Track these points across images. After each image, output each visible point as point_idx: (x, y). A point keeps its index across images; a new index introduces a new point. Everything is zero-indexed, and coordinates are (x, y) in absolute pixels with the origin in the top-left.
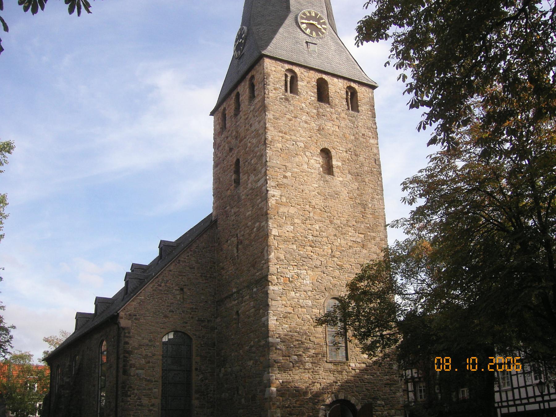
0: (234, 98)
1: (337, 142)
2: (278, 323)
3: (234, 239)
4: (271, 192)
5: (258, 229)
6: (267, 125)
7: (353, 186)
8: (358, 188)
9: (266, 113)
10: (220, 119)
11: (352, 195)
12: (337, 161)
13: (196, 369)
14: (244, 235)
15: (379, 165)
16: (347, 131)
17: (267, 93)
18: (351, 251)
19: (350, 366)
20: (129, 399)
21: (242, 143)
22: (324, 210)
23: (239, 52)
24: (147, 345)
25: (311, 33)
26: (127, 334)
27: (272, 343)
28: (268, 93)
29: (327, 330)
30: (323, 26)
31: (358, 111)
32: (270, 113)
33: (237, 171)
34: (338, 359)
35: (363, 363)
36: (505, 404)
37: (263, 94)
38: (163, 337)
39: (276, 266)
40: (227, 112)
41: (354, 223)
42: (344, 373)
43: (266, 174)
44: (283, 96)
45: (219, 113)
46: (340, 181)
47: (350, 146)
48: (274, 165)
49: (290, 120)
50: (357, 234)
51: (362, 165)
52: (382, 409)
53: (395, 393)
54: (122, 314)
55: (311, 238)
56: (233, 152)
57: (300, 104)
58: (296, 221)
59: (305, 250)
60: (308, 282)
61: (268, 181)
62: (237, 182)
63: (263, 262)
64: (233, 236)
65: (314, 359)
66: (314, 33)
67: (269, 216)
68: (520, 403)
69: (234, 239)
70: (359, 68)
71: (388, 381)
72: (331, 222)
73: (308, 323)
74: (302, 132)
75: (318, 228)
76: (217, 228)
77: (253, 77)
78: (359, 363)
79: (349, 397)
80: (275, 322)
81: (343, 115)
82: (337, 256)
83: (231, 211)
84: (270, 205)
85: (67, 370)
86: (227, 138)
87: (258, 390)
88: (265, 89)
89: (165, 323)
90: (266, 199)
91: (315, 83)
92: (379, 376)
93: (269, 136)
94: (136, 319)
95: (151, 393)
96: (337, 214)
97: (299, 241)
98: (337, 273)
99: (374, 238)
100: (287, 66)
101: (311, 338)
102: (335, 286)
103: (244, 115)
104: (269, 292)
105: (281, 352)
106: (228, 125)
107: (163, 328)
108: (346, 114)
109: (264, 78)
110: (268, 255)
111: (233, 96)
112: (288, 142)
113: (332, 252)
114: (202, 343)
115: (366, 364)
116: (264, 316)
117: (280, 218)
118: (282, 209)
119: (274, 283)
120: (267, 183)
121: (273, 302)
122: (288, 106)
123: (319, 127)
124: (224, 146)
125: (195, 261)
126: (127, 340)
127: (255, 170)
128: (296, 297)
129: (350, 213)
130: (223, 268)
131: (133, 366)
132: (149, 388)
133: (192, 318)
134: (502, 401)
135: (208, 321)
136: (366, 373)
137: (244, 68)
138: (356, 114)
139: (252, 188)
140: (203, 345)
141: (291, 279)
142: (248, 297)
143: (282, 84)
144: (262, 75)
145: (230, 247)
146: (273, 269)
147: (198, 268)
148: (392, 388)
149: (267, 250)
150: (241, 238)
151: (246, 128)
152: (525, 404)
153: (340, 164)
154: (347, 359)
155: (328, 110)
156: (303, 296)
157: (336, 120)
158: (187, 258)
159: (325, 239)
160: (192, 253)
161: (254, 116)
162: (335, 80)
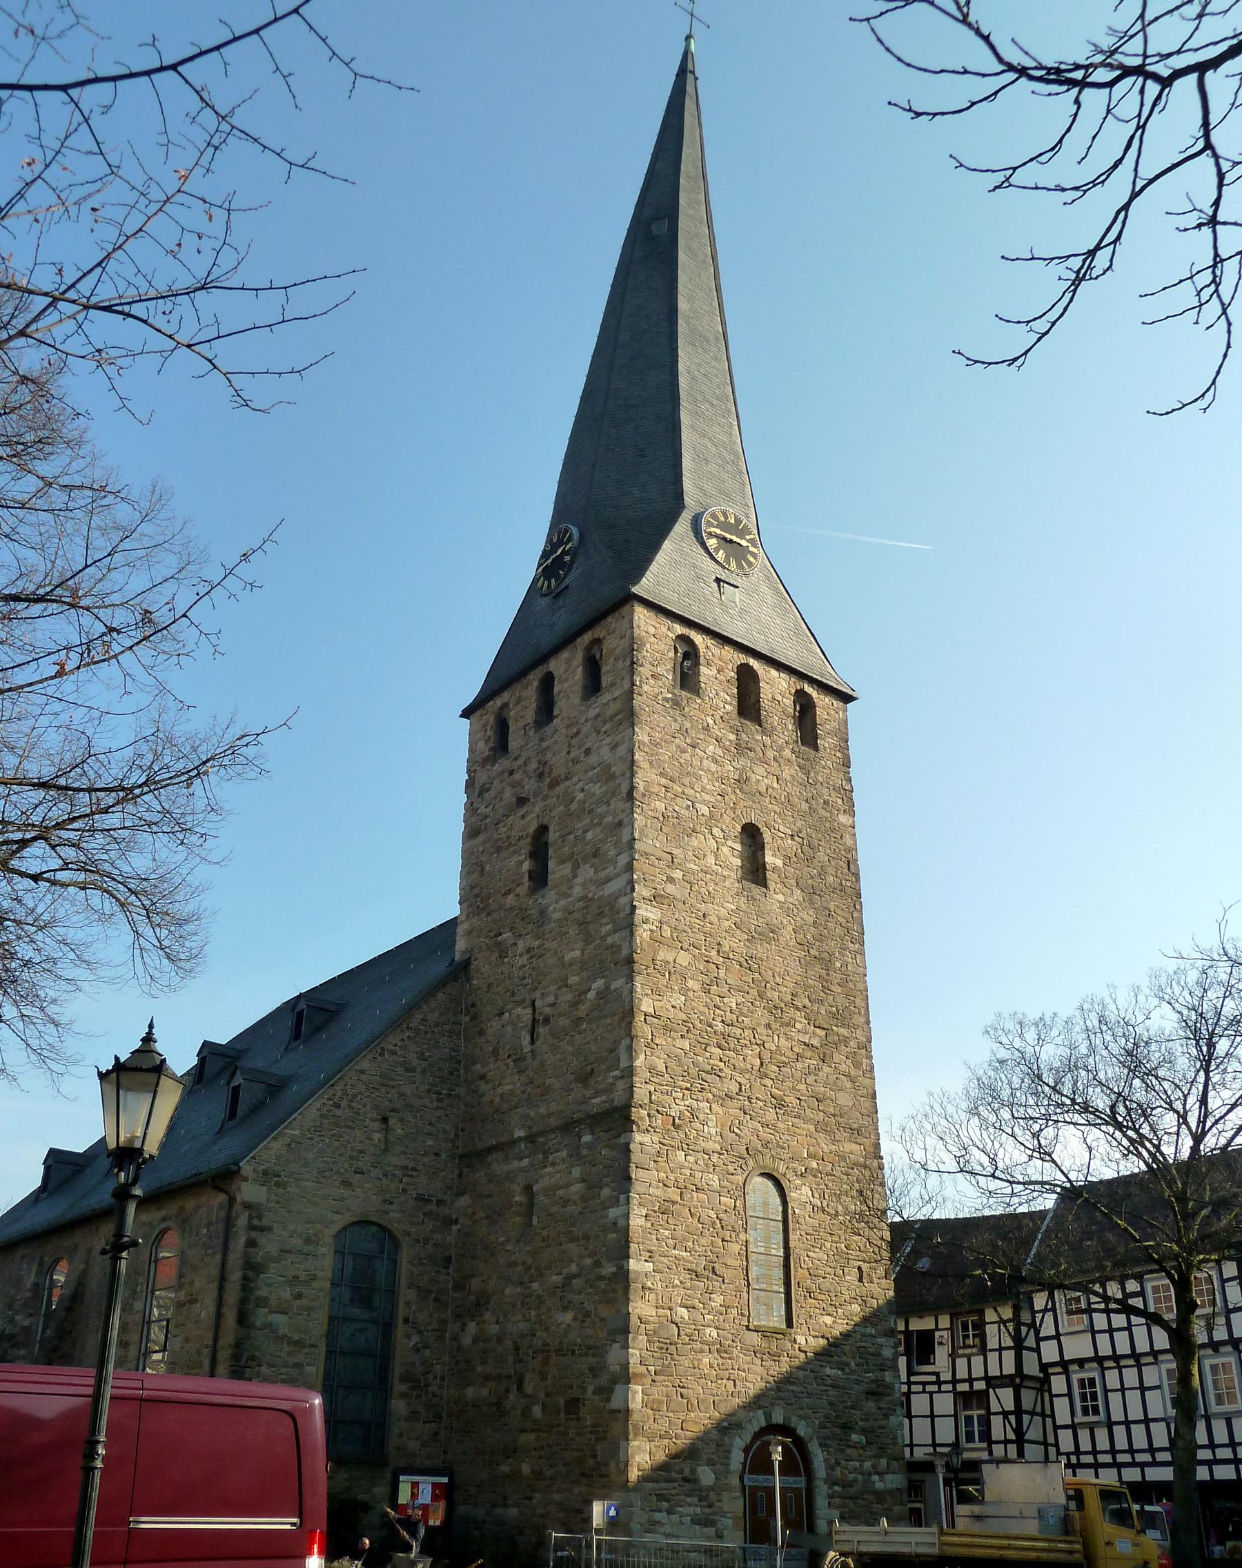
0: (535, 684)
4: (644, 911)
7: (805, 917)
9: (636, 729)
10: (489, 728)
13: (406, 1321)
14: (555, 1004)
15: (857, 875)
17: (638, 683)
18: (800, 1065)
19: (795, 1341)
21: (557, 789)
22: (749, 963)
23: (553, 581)
24: (300, 1252)
25: (727, 560)
26: (255, 1222)
27: (635, 1272)
31: (816, 748)
34: (771, 1324)
35: (823, 1337)
36: (1088, 1459)
39: (648, 1086)
41: (806, 1002)
43: (630, 868)
44: (670, 696)
45: (487, 713)
46: (779, 902)
51: (822, 872)
52: (860, 1456)
53: (886, 1416)
54: (246, 1168)
55: (719, 1027)
60: (713, 1131)
62: (539, 878)
63: (617, 1073)
64: (520, 1003)
65: (721, 1318)
66: (733, 563)
67: (636, 967)
68: (1150, 1460)
69: (525, 1013)
70: (819, 651)
71: (874, 1386)
72: (761, 996)
73: (711, 1229)
74: (705, 781)
75: (734, 1006)
76: (468, 980)
79: (794, 1419)
80: (641, 1221)
81: (787, 753)
82: (772, 1075)
83: (515, 944)
85: (29, 1294)
86: (511, 773)
87: (590, 1389)
88: (633, 674)
89: (342, 1199)
90: (629, 925)
92: (855, 1371)
93: (640, 782)
94: (278, 1184)
95: (298, 1375)
98: (771, 1115)
99: (846, 1041)
100: (679, 629)
102: (766, 1145)
103: (568, 727)
104: (632, 1146)
105: (653, 1296)
106: (514, 743)
107: (337, 1213)
110: (631, 1058)
111: (534, 679)
113: (762, 1064)
114: (423, 1255)
115: (828, 1339)
116: (615, 1202)
117: (658, 975)
118: (664, 955)
120: (633, 890)
122: (679, 719)
124: (502, 792)
125: (416, 1052)
127: (595, 855)
128: (686, 1164)
129: (799, 978)
130: (483, 1077)
131: (262, 1302)
132: (296, 1364)
133: (404, 1191)
135: (440, 1202)
136: (829, 1362)
137: (564, 619)
139: (587, 897)
140: (424, 1261)
141: (677, 1121)
142: (564, 1153)
143: (669, 667)
144: (625, 643)
147: (424, 1072)
148: (883, 1405)
150: (547, 1010)
151: (572, 755)
152: (1142, 1465)
153: (779, 863)
154: (790, 1323)
156: (701, 1162)
158: (399, 1044)
159: (747, 1032)
160: (412, 1035)
162: (774, 673)
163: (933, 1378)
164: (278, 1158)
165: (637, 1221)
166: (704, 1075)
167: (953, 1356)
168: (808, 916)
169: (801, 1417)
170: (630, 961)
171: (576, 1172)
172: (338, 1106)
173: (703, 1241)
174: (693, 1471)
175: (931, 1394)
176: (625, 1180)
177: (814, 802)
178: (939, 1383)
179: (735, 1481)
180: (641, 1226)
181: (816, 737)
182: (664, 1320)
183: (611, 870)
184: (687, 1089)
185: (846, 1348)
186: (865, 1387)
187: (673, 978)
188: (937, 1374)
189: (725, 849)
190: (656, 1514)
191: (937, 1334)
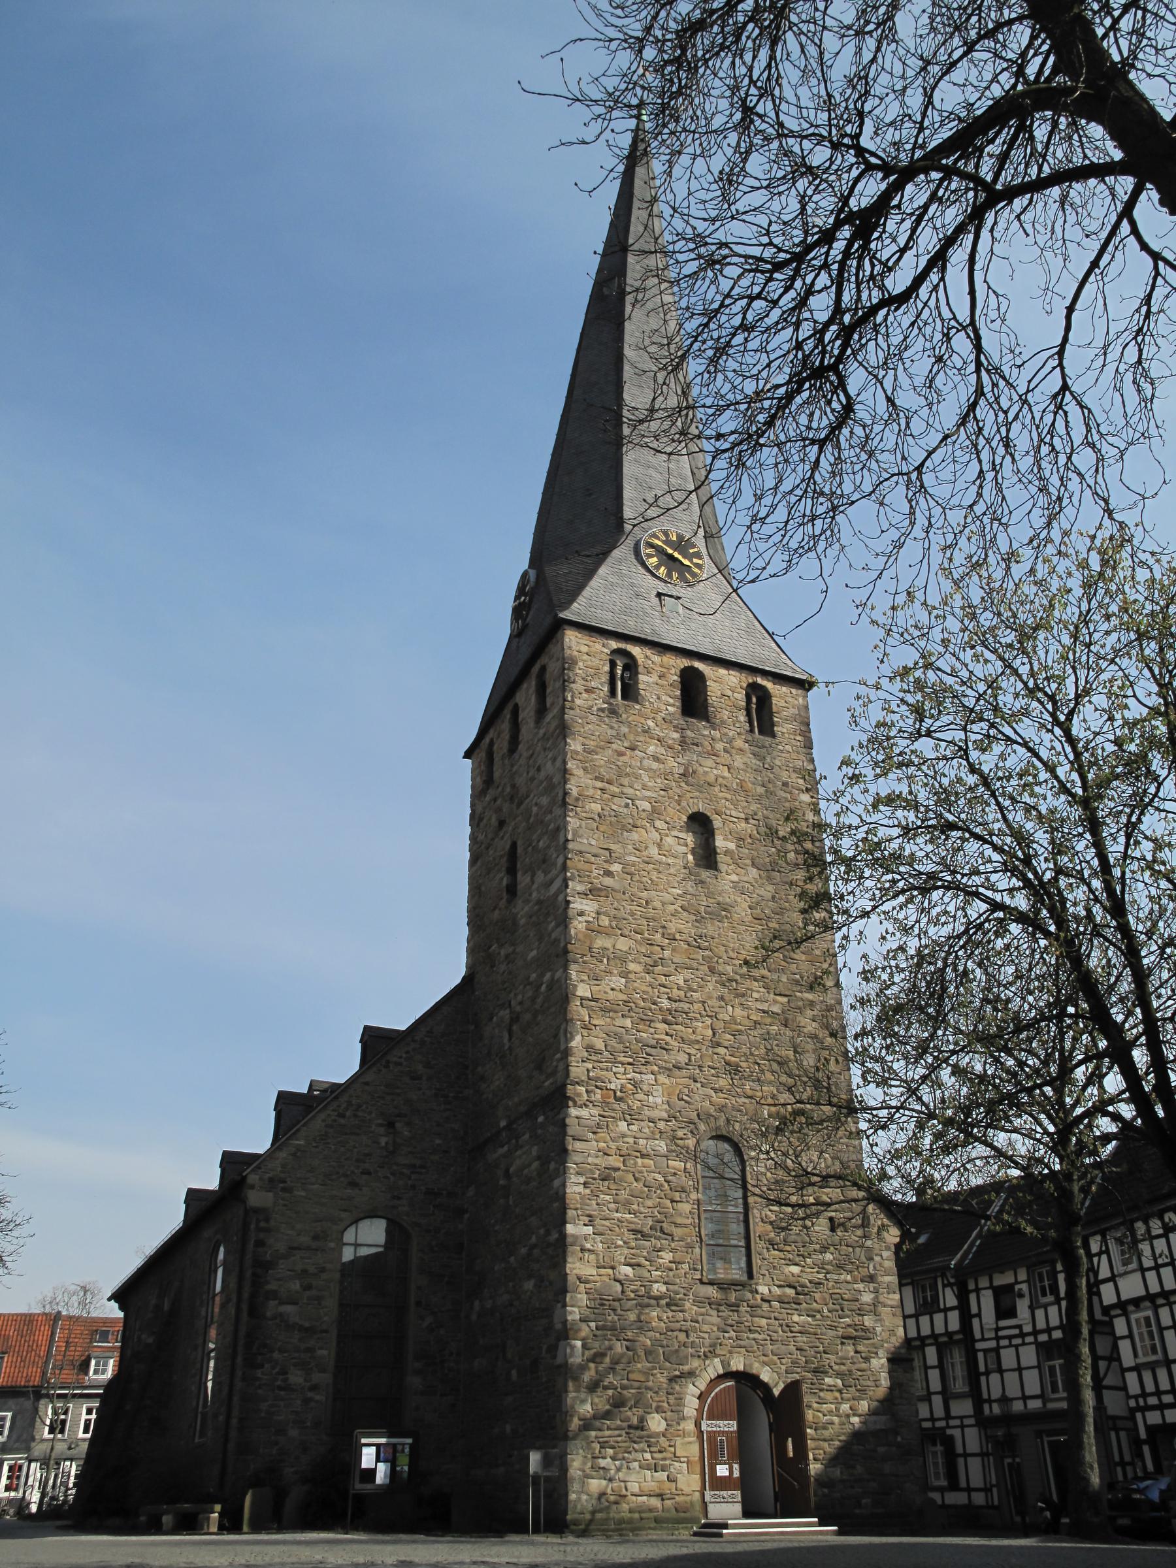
0: (508, 716)
1: (726, 799)
2: (588, 1191)
3: (505, 1014)
4: (577, 904)
5: (550, 987)
6: (569, 765)
7: (762, 892)
8: (773, 897)
11: (759, 911)
12: (726, 839)
13: (418, 1304)
16: (748, 777)
20: (259, 1373)
21: (522, 807)
24: (308, 1248)
25: (669, 575)
26: (262, 1224)
27: (573, 1235)
28: (573, 701)
29: (702, 1208)
30: (695, 561)
31: (773, 735)
32: (574, 739)
33: (512, 870)
34: (730, 1277)
35: (790, 1286)
36: (1153, 1401)
37: (561, 702)
38: (345, 1230)
40: (495, 748)
42: (744, 1308)
43: (565, 868)
47: (754, 807)
48: (583, 848)
49: (621, 754)
50: (772, 996)
53: (867, 1359)
55: (665, 1003)
56: (504, 829)
57: (643, 721)
58: (632, 966)
59: (652, 1030)
60: (659, 1100)
61: (570, 883)
62: (512, 890)
63: (558, 1056)
64: (502, 1006)
65: (671, 1274)
66: (675, 575)
67: (570, 956)
69: (505, 1014)
71: (851, 1330)
72: (712, 970)
74: (646, 778)
75: (681, 982)
77: (543, 669)
78: (779, 1286)
80: (580, 1189)
81: (739, 743)
82: (726, 1043)
84: (573, 932)
88: (564, 690)
90: (564, 921)
91: (676, 678)
93: (573, 788)
94: (284, 1190)
96: (727, 952)
97: (637, 1010)
98: (723, 1082)
99: (812, 1004)
100: (614, 644)
101: (665, 1225)
104: (568, 1121)
105: (592, 1257)
107: (345, 1210)
108: (746, 741)
109: (564, 669)
110: (568, 1041)
111: (507, 714)
112: (616, 800)
113: (714, 1034)
116: (557, 1176)
118: (600, 942)
119: (579, 1103)
120: (567, 886)
121: (578, 1145)
123: (686, 770)
124: (490, 819)
126: (262, 1235)
127: (544, 861)
131: (274, 1295)
133: (413, 1187)
134: (1144, 1395)
138: (767, 740)
141: (618, 1094)
142: (527, 1136)
143: (604, 680)
144: (560, 663)
145: (497, 1031)
146: (578, 1070)
148: (861, 1348)
149: (566, 1030)
150: (518, 1009)
153: (732, 846)
154: (750, 1275)
155: (706, 733)
157: (722, 753)
159: (697, 1006)
161: (545, 749)
162: (722, 671)
163: (1017, 1331)
164: (284, 1166)
165: (575, 1187)
166: (648, 1050)
167: (1032, 1309)
168: (767, 891)
169: (765, 1364)
170: (566, 952)
171: (535, 1151)
172: (342, 1116)
173: (649, 1203)
174: (642, 1420)
175: (1016, 1347)
176: (563, 1153)
177: (770, 786)
178: (1022, 1335)
179: (690, 1426)
180: (580, 1193)
181: (773, 725)
182: (606, 1279)
183: (554, 872)
184: (630, 1064)
185: (817, 1296)
186: (841, 1332)
187: (611, 962)
188: (1020, 1327)
189: (669, 840)
190: (600, 1460)
191: (1017, 1287)
